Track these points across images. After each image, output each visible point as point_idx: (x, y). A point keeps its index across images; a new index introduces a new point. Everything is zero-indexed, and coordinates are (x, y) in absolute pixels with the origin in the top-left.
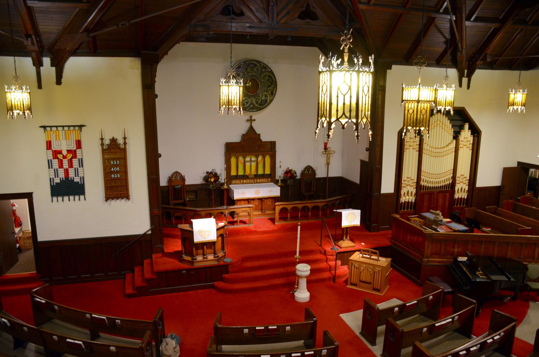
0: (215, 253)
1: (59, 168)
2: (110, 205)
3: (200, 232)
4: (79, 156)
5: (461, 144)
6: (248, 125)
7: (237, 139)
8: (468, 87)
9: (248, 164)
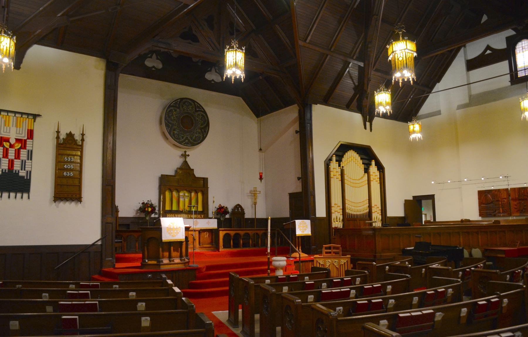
0: (181, 256)
1: (3, 157)
2: (57, 207)
3: (169, 229)
4: (29, 147)
5: (372, 178)
6: (181, 160)
7: (170, 171)
8: (371, 130)
9: (181, 200)
